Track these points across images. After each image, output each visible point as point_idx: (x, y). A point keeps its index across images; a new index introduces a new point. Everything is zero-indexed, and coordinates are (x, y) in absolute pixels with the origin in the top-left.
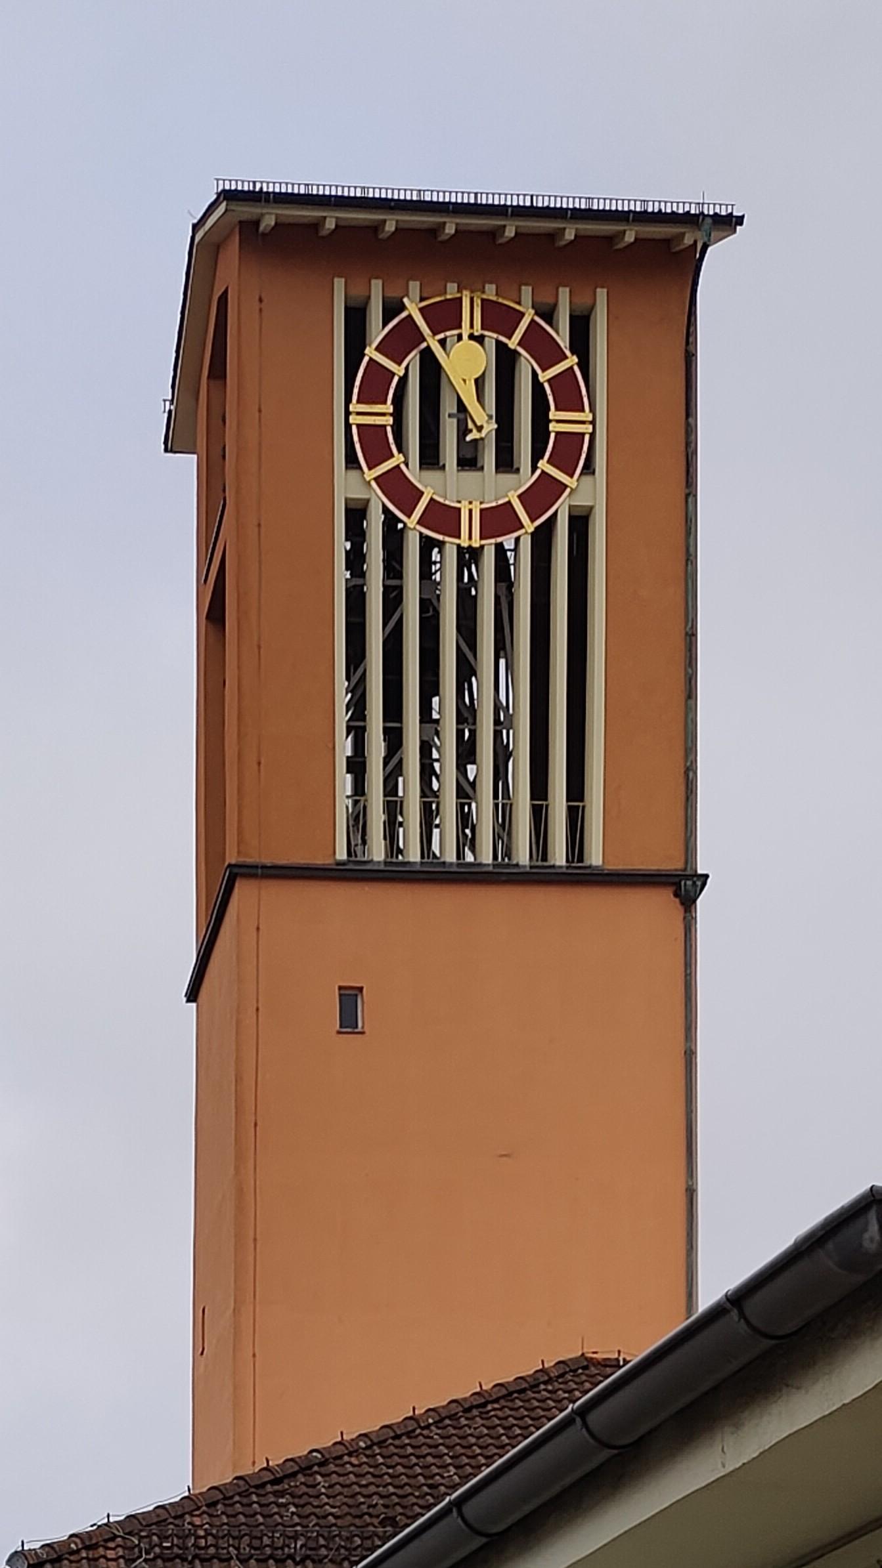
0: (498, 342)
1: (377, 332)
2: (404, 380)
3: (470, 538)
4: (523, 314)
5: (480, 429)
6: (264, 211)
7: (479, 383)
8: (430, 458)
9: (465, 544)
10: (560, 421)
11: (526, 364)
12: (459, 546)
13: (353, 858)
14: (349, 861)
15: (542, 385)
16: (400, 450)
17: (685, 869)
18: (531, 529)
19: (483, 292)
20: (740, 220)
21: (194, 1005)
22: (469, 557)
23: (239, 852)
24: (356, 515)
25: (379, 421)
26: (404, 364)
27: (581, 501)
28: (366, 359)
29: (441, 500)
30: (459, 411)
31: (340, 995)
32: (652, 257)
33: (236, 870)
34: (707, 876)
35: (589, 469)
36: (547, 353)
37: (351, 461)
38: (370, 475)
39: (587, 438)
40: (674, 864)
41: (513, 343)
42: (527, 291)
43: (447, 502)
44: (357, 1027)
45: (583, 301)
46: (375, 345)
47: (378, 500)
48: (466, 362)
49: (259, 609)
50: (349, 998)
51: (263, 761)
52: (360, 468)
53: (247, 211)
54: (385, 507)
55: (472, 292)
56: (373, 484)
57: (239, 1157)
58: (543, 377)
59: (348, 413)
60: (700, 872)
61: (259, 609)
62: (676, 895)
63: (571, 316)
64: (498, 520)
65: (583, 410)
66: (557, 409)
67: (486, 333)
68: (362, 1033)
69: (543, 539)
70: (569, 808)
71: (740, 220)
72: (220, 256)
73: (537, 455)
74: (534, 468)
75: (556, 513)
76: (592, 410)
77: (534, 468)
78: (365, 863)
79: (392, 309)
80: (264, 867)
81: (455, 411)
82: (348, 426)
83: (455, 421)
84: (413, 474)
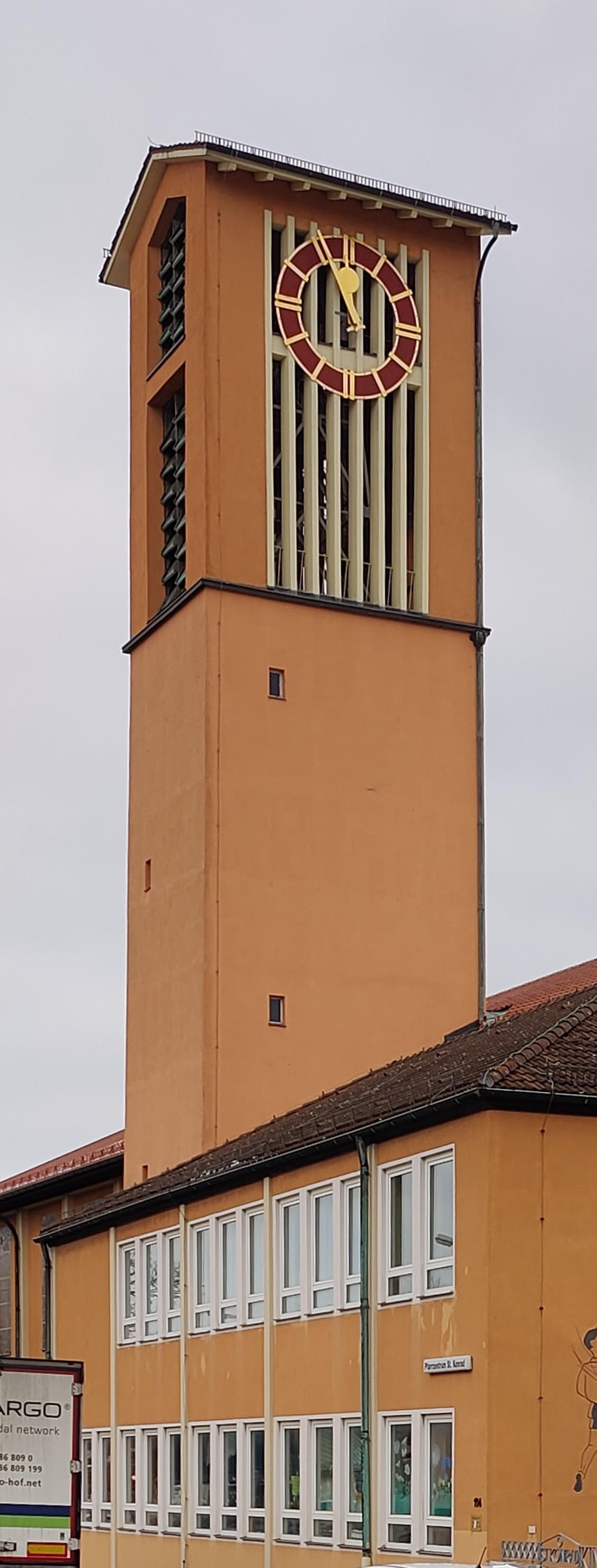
0: (365, 272)
1: (291, 251)
2: (307, 285)
3: (349, 393)
4: (379, 258)
5: (355, 325)
6: (225, 159)
7: (355, 295)
8: (322, 339)
9: (346, 397)
10: (401, 329)
11: (381, 290)
12: (342, 398)
13: (278, 586)
14: (276, 588)
15: (390, 304)
16: (306, 330)
17: (476, 624)
18: (385, 395)
19: (356, 237)
20: (515, 228)
21: (129, 655)
22: (347, 405)
23: (207, 571)
24: (278, 363)
25: (293, 308)
26: (308, 274)
27: (415, 382)
28: (284, 267)
29: (331, 366)
30: (342, 310)
31: (271, 674)
32: (456, 236)
33: (206, 583)
34: (489, 631)
35: (418, 363)
36: (395, 286)
37: (276, 330)
38: (288, 341)
39: (418, 343)
40: (470, 620)
41: (374, 274)
42: (381, 243)
43: (335, 368)
44: (278, 695)
45: (415, 256)
46: (291, 258)
47: (292, 360)
48: (348, 280)
49: (219, 414)
50: (275, 676)
51: (222, 514)
52: (281, 335)
53: (215, 156)
54: (297, 365)
55: (350, 236)
56: (289, 347)
57: (208, 771)
58: (392, 299)
59: (274, 299)
60: (485, 626)
61: (219, 414)
62: (471, 639)
63: (408, 264)
64: (365, 384)
65: (296, 297)
66: (281, 293)
67: (357, 264)
68: (284, 700)
69: (390, 401)
70: (298, 553)
71: (515, 228)
72: (166, 175)
73: (388, 348)
74: (387, 356)
75: (399, 388)
76: (421, 326)
77: (387, 356)
78: (351, 602)
79: (300, 238)
80: (224, 584)
81: (339, 310)
82: (274, 308)
83: (339, 317)
84: (314, 345)
